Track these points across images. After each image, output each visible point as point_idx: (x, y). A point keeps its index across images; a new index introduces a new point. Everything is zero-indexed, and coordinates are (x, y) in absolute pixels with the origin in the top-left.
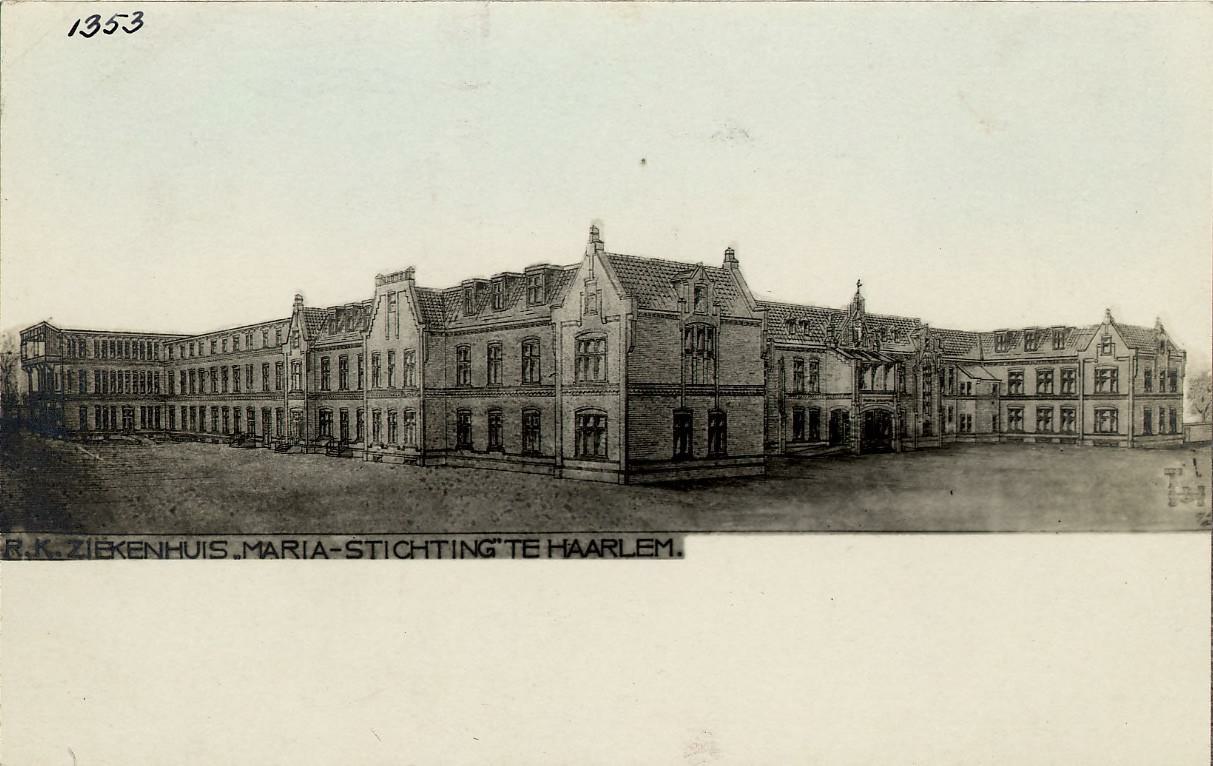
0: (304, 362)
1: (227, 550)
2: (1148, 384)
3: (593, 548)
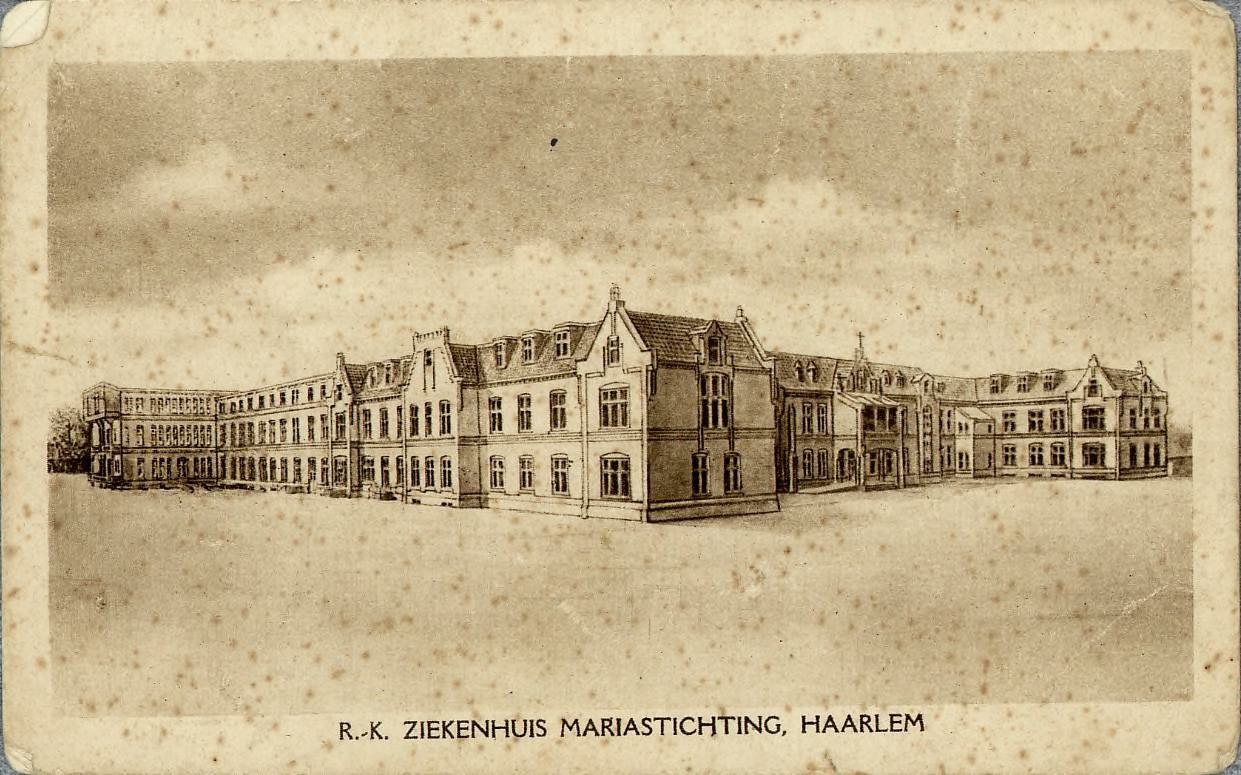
0: (347, 415)
1: (651, 726)
2: (1133, 421)
3: (631, 726)
